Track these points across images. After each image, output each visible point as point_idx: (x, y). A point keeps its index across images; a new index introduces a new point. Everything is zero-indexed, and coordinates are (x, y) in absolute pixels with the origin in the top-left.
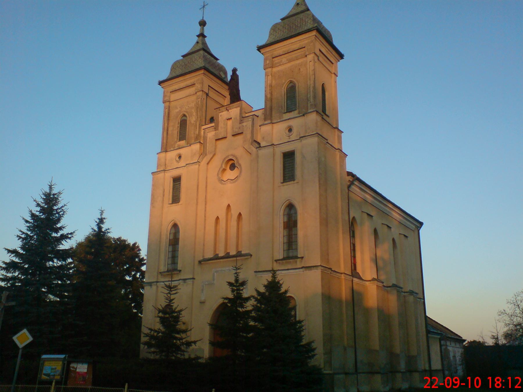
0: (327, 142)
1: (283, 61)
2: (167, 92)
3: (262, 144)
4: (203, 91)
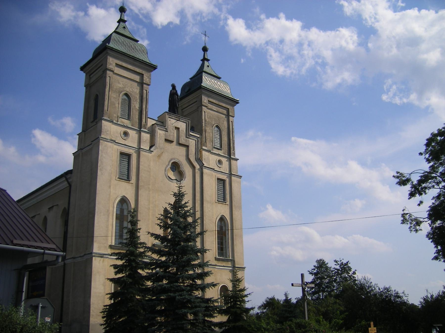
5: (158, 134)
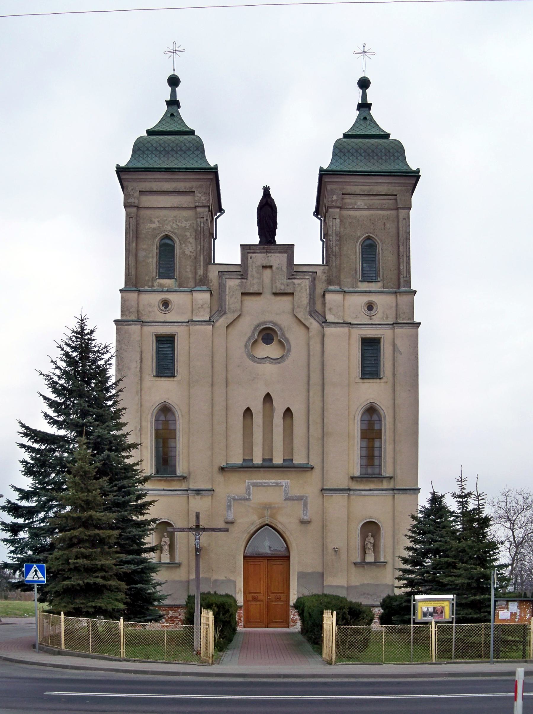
1: (359, 203)
5: (227, 288)
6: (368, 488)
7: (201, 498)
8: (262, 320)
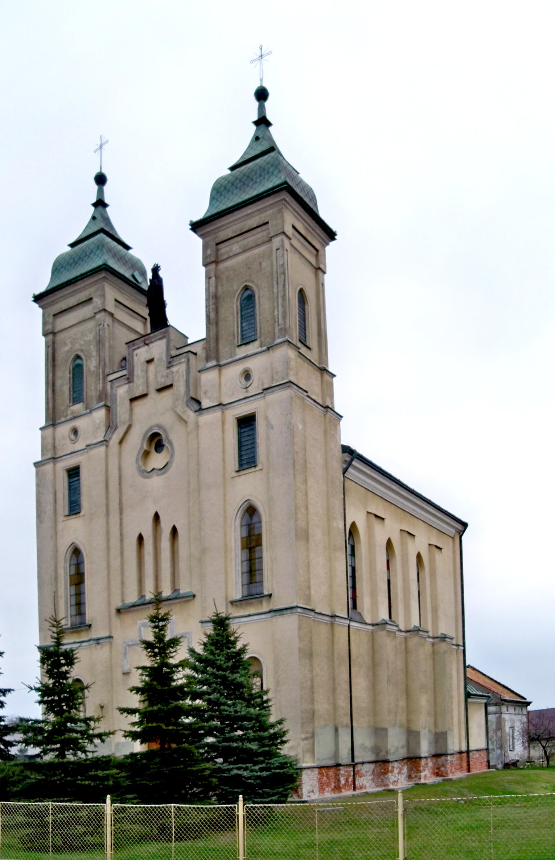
0: (308, 396)
2: (48, 315)
3: (205, 404)
4: (105, 310)
6: (247, 613)
7: (101, 648)
8: (149, 426)
